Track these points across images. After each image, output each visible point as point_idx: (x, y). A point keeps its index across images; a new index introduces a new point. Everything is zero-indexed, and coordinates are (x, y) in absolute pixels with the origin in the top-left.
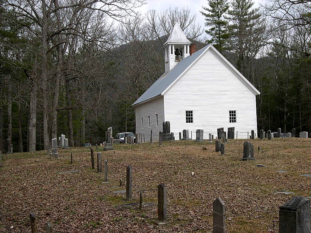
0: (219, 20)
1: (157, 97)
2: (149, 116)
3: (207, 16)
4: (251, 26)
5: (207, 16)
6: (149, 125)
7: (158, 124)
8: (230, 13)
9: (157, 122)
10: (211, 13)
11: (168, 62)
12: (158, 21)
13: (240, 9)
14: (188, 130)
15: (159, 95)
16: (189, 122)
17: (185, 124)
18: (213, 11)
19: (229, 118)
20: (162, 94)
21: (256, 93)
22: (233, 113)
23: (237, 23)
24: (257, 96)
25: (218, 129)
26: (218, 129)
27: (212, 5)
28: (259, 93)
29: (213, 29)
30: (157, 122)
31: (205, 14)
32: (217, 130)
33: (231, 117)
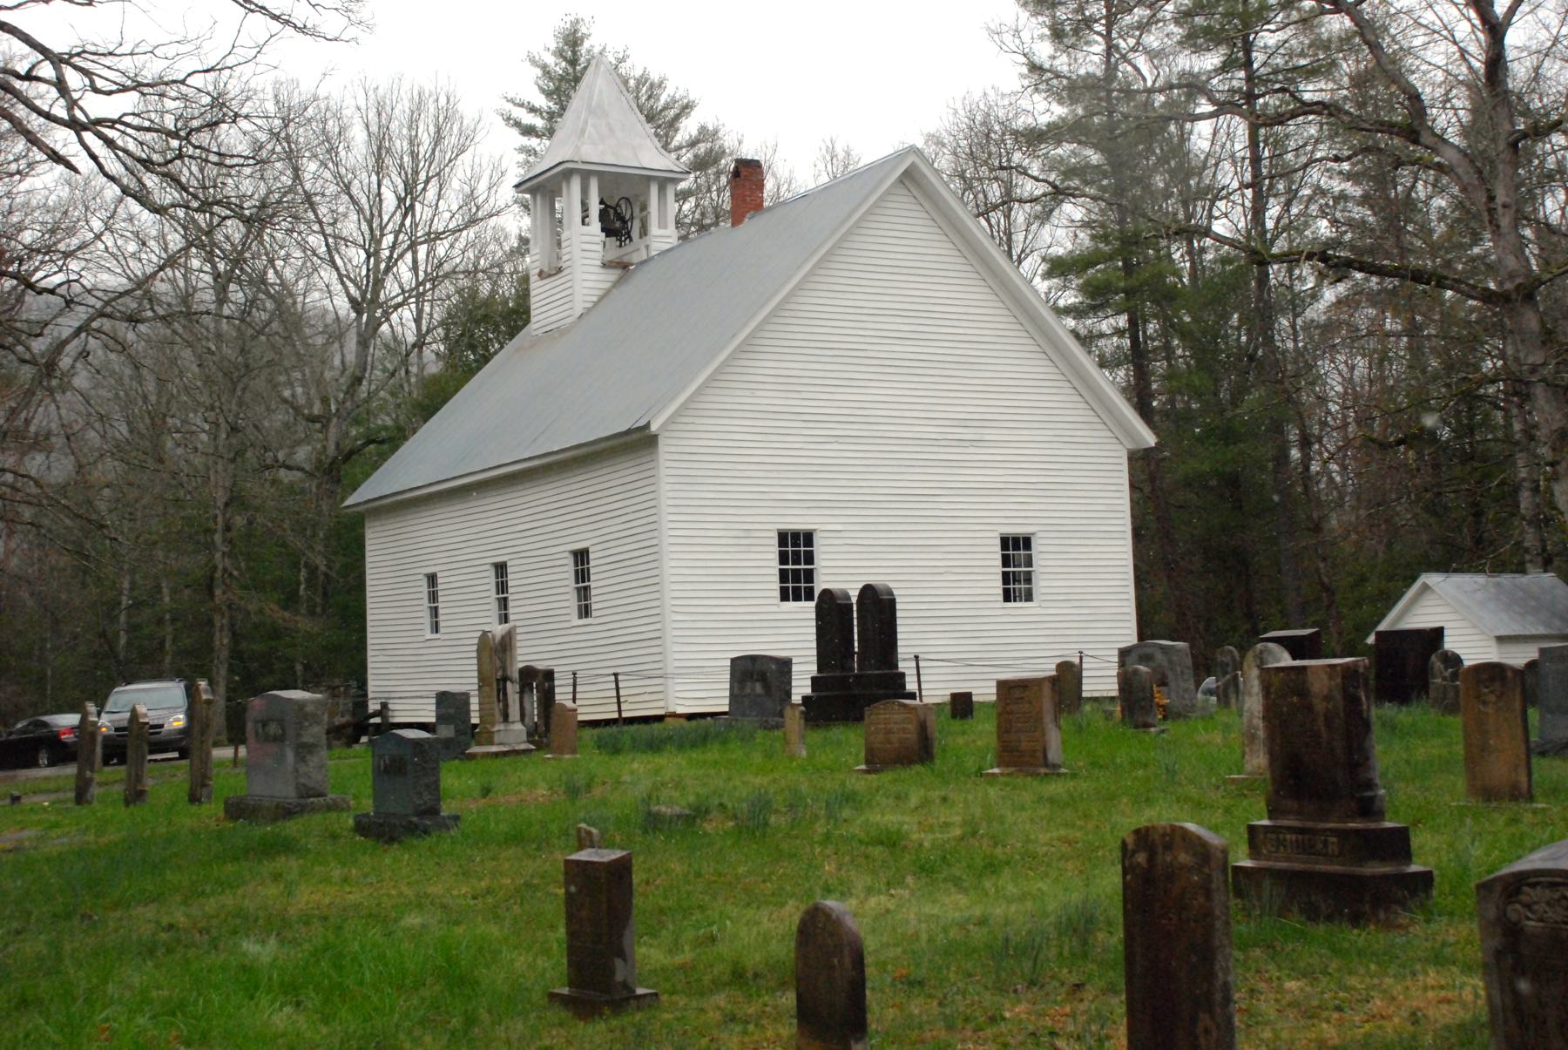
16: (797, 598)
17: (774, 609)
19: (1000, 577)
24: (1141, 462)
28: (1150, 439)
31: (517, 124)
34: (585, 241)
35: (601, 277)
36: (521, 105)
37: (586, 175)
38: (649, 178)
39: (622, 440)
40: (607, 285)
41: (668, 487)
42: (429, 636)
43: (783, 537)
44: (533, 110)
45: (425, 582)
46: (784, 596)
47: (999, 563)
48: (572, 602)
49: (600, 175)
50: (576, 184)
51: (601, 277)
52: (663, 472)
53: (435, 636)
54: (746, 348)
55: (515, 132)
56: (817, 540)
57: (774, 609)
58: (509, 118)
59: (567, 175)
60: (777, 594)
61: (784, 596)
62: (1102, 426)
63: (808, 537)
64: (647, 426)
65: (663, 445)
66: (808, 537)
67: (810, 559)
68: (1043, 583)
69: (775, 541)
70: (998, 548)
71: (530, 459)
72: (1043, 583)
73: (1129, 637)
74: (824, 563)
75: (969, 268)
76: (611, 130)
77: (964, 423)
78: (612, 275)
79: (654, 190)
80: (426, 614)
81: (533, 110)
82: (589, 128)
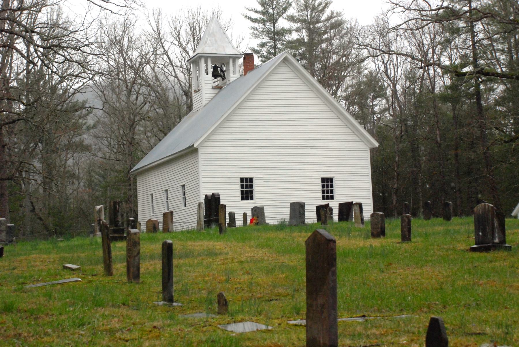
0: (274, 27)
1: (182, 153)
2: (167, 191)
3: (255, 21)
4: (329, 40)
5: (255, 21)
6: (151, 210)
7: (168, 207)
8: (291, 19)
9: (153, 208)
10: (258, 16)
11: (199, 90)
12: (166, 30)
13: (309, 12)
14: (304, 203)
15: (190, 147)
16: (247, 199)
17: (239, 203)
18: (263, 13)
19: (321, 192)
20: (195, 146)
21: (371, 143)
22: (327, 181)
23: (305, 35)
24: (373, 151)
25: (317, 207)
26: (317, 207)
27: (263, 4)
28: (377, 144)
29: (263, 45)
30: (153, 208)
31: (249, 18)
32: (315, 208)
33: (325, 189)
34: (206, 81)
35: (211, 92)
36: (252, 10)
37: (206, 58)
38: (230, 57)
39: (185, 152)
40: (214, 95)
41: (202, 164)
42: (183, 208)
43: (242, 180)
44: (256, 12)
45: (181, 188)
46: (243, 199)
47: (321, 187)
48: (182, 202)
49: (212, 57)
50: (203, 61)
51: (211, 92)
52: (200, 160)
53: (185, 208)
54: (228, 119)
55: (249, 21)
56: (254, 180)
57: (239, 203)
58: (246, 16)
59: (200, 57)
60: (240, 198)
61: (243, 199)
62: (360, 140)
63: (251, 180)
64: (193, 145)
65: (200, 152)
66: (251, 180)
67: (251, 186)
68: (337, 194)
69: (239, 181)
70: (320, 182)
71: (168, 156)
72: (337, 194)
73: (372, 212)
74: (336, 182)
75: (309, 89)
76: (216, 41)
77: (307, 141)
78: (216, 91)
79: (231, 61)
80: (182, 200)
81: (256, 12)
82: (208, 41)
